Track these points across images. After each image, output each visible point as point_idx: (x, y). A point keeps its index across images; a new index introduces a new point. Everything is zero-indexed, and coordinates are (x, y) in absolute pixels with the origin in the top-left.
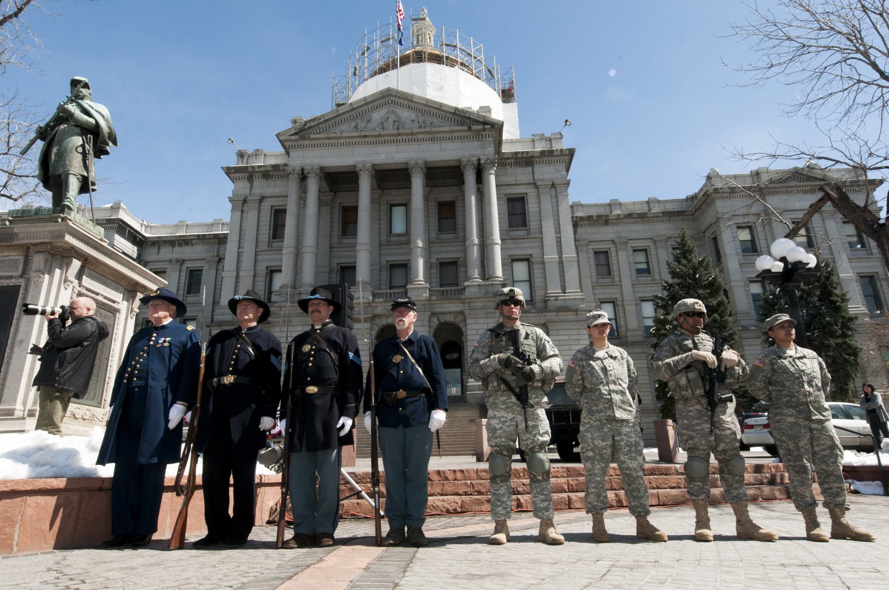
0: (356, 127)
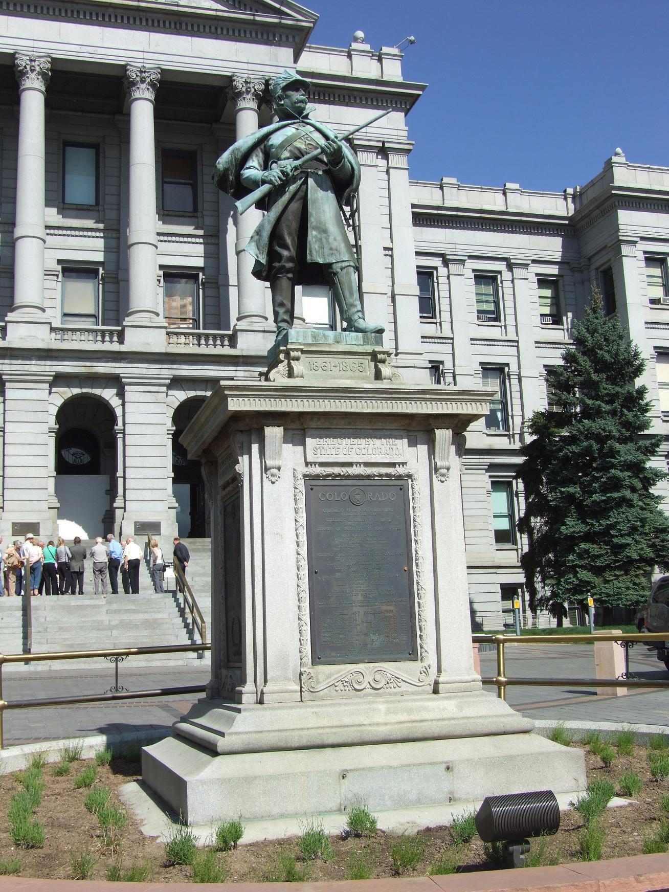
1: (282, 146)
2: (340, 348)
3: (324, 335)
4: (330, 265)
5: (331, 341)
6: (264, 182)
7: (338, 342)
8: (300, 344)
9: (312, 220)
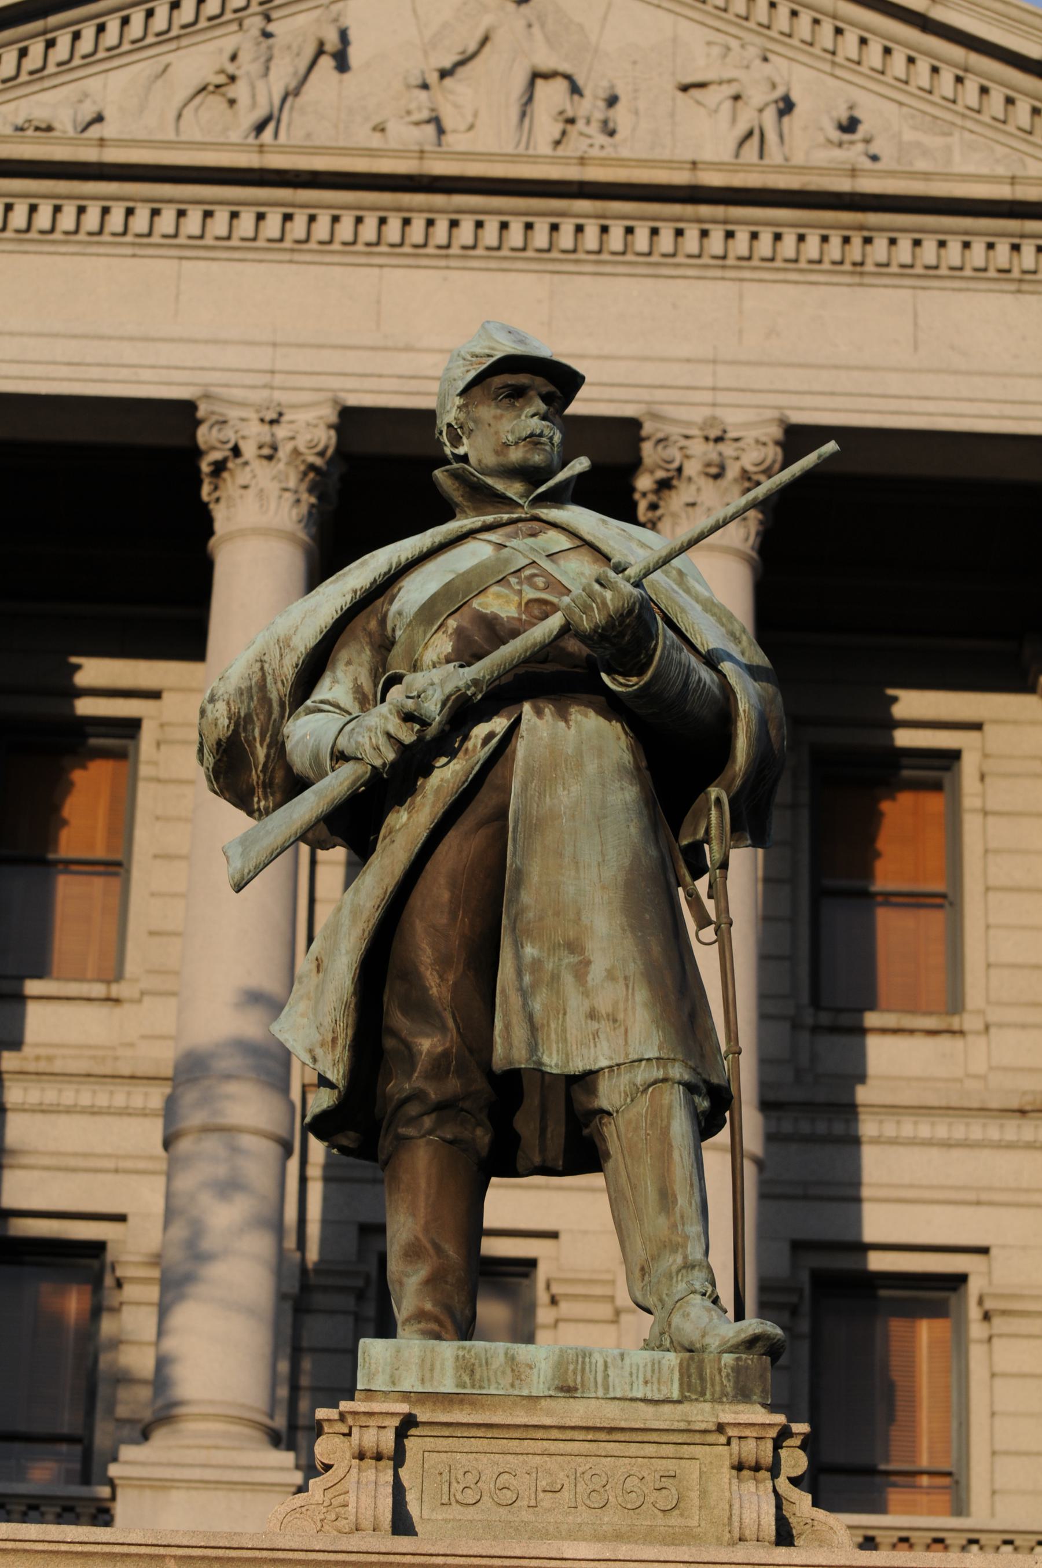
0: (221, 87)
1: (429, 613)
2: (577, 1412)
3: (511, 1359)
4: (587, 1080)
5: (539, 1383)
6: (340, 757)
7: (568, 1391)
8: (406, 1396)
9: (530, 898)
